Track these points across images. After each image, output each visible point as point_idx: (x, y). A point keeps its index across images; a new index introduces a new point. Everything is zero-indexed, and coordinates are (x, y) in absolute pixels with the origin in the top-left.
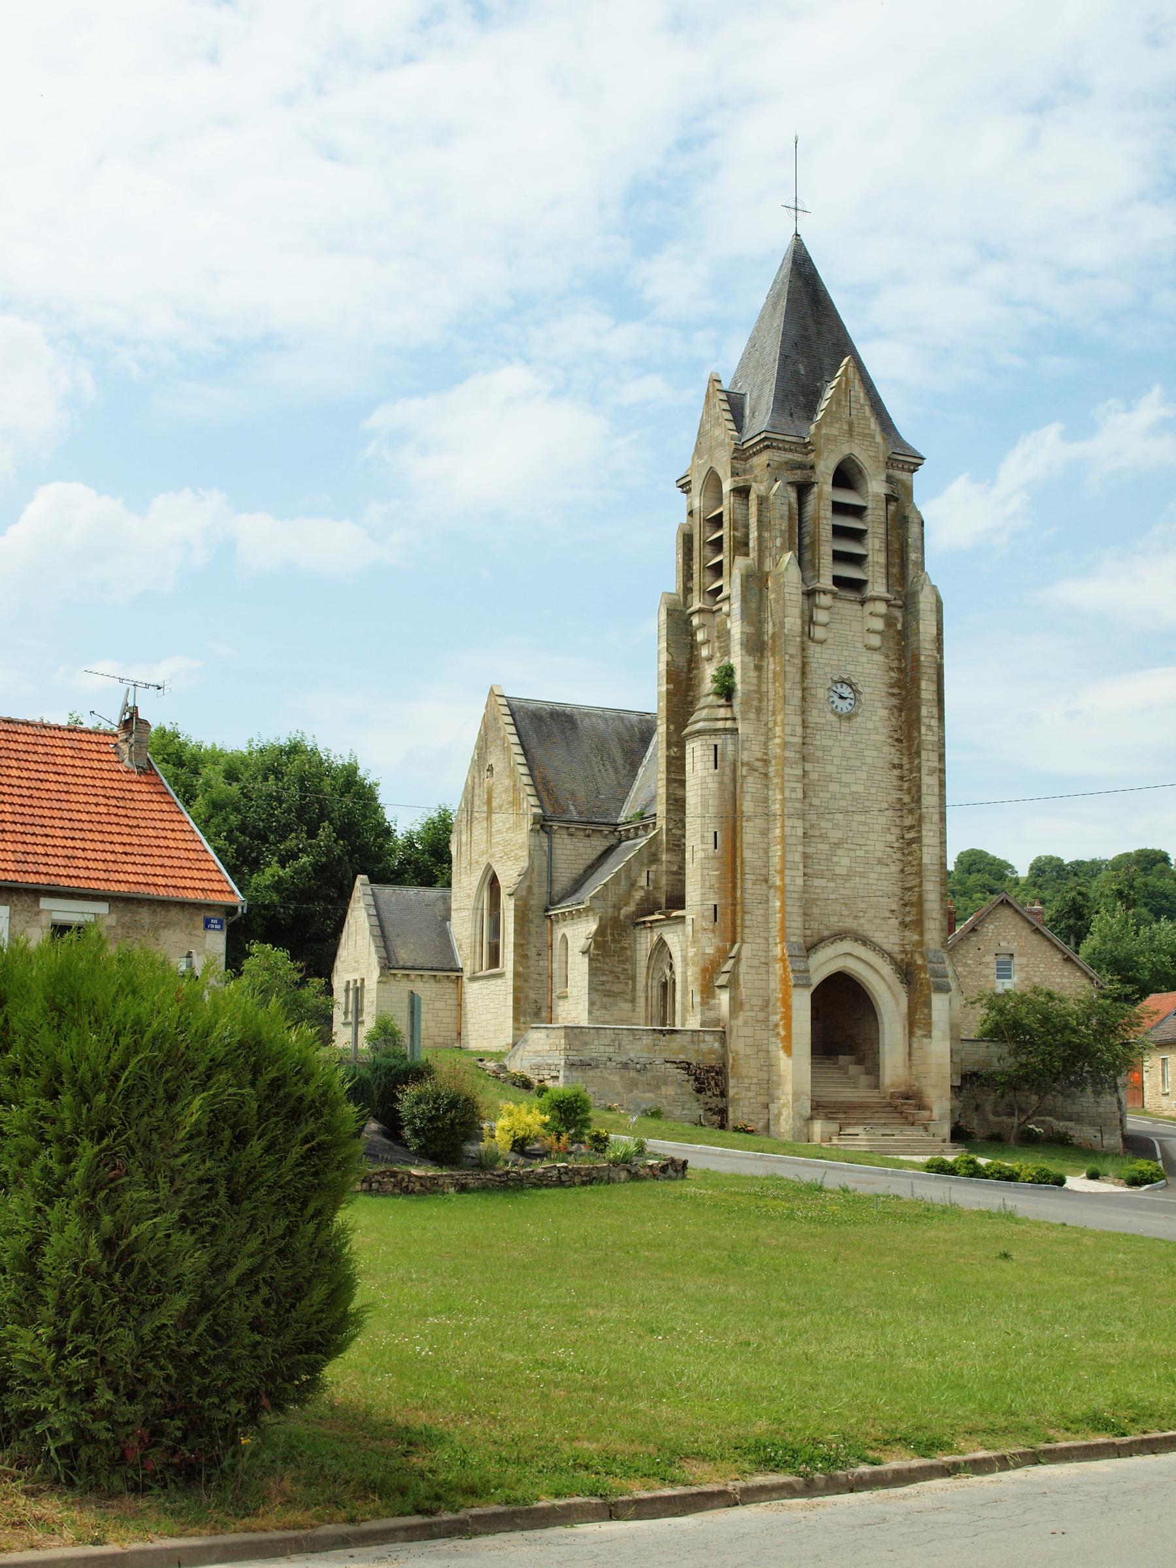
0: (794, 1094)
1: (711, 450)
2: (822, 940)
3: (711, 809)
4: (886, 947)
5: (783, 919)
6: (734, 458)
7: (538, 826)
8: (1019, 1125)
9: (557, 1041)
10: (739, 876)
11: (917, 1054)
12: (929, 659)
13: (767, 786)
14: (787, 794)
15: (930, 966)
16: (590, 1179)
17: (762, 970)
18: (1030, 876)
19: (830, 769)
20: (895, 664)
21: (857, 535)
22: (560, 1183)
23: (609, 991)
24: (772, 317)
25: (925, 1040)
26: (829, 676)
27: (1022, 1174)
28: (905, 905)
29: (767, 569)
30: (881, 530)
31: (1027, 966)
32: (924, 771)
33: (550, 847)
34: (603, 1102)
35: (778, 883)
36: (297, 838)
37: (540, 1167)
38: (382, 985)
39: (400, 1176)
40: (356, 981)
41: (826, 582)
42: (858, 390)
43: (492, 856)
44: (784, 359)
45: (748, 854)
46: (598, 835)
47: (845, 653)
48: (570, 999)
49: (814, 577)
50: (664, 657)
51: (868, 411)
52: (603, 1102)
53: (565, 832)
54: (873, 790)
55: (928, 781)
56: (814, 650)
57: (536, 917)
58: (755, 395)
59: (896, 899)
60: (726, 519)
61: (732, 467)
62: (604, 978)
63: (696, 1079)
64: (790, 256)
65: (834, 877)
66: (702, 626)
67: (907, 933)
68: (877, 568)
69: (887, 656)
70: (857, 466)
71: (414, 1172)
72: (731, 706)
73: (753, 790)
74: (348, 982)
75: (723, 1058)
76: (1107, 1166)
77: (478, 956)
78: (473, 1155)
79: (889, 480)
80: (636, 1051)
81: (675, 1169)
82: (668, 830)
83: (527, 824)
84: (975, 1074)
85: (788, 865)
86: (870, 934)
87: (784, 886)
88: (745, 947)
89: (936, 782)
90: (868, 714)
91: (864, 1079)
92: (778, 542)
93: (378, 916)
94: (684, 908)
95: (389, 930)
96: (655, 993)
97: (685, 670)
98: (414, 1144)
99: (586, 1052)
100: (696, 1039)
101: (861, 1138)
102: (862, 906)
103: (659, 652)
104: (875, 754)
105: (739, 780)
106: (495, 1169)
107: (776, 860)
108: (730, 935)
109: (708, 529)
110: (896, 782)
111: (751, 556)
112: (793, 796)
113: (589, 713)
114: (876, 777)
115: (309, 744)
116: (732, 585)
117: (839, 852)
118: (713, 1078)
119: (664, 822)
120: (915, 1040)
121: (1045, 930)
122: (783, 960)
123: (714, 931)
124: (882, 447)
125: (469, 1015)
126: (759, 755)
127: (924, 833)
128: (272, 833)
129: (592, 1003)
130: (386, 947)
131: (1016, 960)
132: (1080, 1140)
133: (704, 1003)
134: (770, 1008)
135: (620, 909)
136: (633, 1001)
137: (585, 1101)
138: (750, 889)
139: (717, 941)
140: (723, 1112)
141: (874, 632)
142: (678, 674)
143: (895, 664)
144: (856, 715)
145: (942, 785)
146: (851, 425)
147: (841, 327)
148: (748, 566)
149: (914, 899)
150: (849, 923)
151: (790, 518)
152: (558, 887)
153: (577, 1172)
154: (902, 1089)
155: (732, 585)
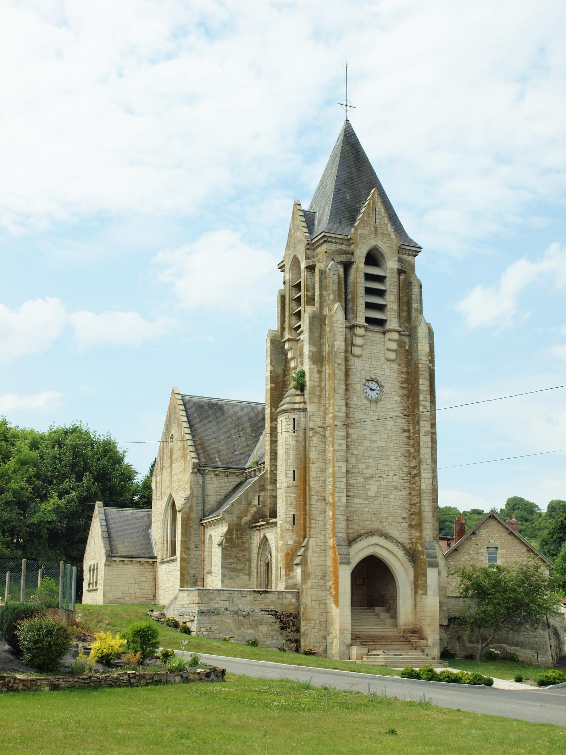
0: (340, 630)
1: (295, 244)
2: (360, 536)
3: (291, 457)
4: (400, 540)
5: (334, 523)
6: (307, 249)
7: (196, 470)
8: (482, 649)
9: (194, 598)
10: (307, 497)
11: (419, 605)
12: (425, 366)
13: (325, 443)
14: (336, 447)
15: (426, 551)
16: (156, 681)
17: (322, 554)
18: (548, 512)
19: (365, 432)
20: (405, 370)
21: (381, 293)
22: (130, 684)
23: (234, 568)
24: (332, 168)
25: (424, 597)
26: (364, 377)
27: (463, 678)
28: (412, 514)
29: (325, 313)
30: (395, 290)
31: (506, 554)
32: (422, 433)
33: (204, 483)
34: (221, 635)
35: (331, 501)
36: (70, 482)
37: (115, 673)
38: (107, 567)
39: (7, 680)
40: (94, 565)
41: (361, 321)
42: (380, 208)
43: (172, 489)
44: (337, 190)
45: (312, 483)
46: (233, 475)
47: (374, 363)
48: (213, 574)
49: (353, 318)
50: (269, 368)
51: (386, 220)
52: (221, 635)
53: (213, 473)
54: (391, 445)
55: (425, 440)
56: (354, 361)
57: (194, 524)
58: (321, 213)
59: (406, 511)
60: (302, 285)
61: (306, 254)
62: (231, 561)
63: (281, 621)
64: (343, 133)
65: (367, 498)
66: (291, 349)
67: (413, 531)
68: (392, 313)
69: (399, 365)
70: (380, 252)
71: (19, 676)
72: (304, 395)
73: (317, 445)
74: (91, 566)
75: (298, 608)
76: (530, 673)
77: (165, 549)
78: (67, 665)
79: (400, 260)
80: (243, 604)
81: (218, 675)
83: (190, 469)
84: (455, 618)
85: (337, 490)
86: (390, 532)
87: (334, 502)
88: (312, 540)
89: (430, 439)
90: (387, 399)
91: (389, 621)
92: (331, 297)
93: (107, 526)
94: (276, 517)
95: (113, 534)
96: (262, 570)
97: (282, 376)
98: (27, 657)
99: (211, 604)
100: (281, 596)
101: (380, 657)
102: (385, 515)
103: (266, 365)
104: (392, 423)
105: (308, 439)
106: (81, 675)
107: (330, 487)
108: (302, 533)
109: (294, 292)
110: (406, 440)
111: (316, 306)
112: (340, 448)
113: (232, 404)
114: (393, 437)
115: (84, 428)
116: (305, 324)
118: (291, 620)
119: (269, 466)
120: (418, 596)
121: (516, 533)
122: (334, 548)
123: (293, 531)
124: (395, 241)
125: (160, 585)
126: (320, 424)
127: (422, 470)
128: (55, 479)
129: (223, 576)
130: (110, 544)
131: (500, 551)
132: (524, 658)
133: (287, 574)
134: (327, 578)
135: (241, 519)
136: (249, 574)
137: (154, 631)
138: (315, 505)
139: (294, 537)
140: (297, 642)
141: (391, 350)
142: (277, 378)
143: (405, 370)
144: (380, 400)
145: (434, 441)
146: (376, 228)
147: (373, 173)
148: (313, 312)
149: (417, 510)
150: (376, 526)
151: (339, 283)
152: (208, 507)
153: (143, 677)
154: (411, 627)
155: (305, 324)
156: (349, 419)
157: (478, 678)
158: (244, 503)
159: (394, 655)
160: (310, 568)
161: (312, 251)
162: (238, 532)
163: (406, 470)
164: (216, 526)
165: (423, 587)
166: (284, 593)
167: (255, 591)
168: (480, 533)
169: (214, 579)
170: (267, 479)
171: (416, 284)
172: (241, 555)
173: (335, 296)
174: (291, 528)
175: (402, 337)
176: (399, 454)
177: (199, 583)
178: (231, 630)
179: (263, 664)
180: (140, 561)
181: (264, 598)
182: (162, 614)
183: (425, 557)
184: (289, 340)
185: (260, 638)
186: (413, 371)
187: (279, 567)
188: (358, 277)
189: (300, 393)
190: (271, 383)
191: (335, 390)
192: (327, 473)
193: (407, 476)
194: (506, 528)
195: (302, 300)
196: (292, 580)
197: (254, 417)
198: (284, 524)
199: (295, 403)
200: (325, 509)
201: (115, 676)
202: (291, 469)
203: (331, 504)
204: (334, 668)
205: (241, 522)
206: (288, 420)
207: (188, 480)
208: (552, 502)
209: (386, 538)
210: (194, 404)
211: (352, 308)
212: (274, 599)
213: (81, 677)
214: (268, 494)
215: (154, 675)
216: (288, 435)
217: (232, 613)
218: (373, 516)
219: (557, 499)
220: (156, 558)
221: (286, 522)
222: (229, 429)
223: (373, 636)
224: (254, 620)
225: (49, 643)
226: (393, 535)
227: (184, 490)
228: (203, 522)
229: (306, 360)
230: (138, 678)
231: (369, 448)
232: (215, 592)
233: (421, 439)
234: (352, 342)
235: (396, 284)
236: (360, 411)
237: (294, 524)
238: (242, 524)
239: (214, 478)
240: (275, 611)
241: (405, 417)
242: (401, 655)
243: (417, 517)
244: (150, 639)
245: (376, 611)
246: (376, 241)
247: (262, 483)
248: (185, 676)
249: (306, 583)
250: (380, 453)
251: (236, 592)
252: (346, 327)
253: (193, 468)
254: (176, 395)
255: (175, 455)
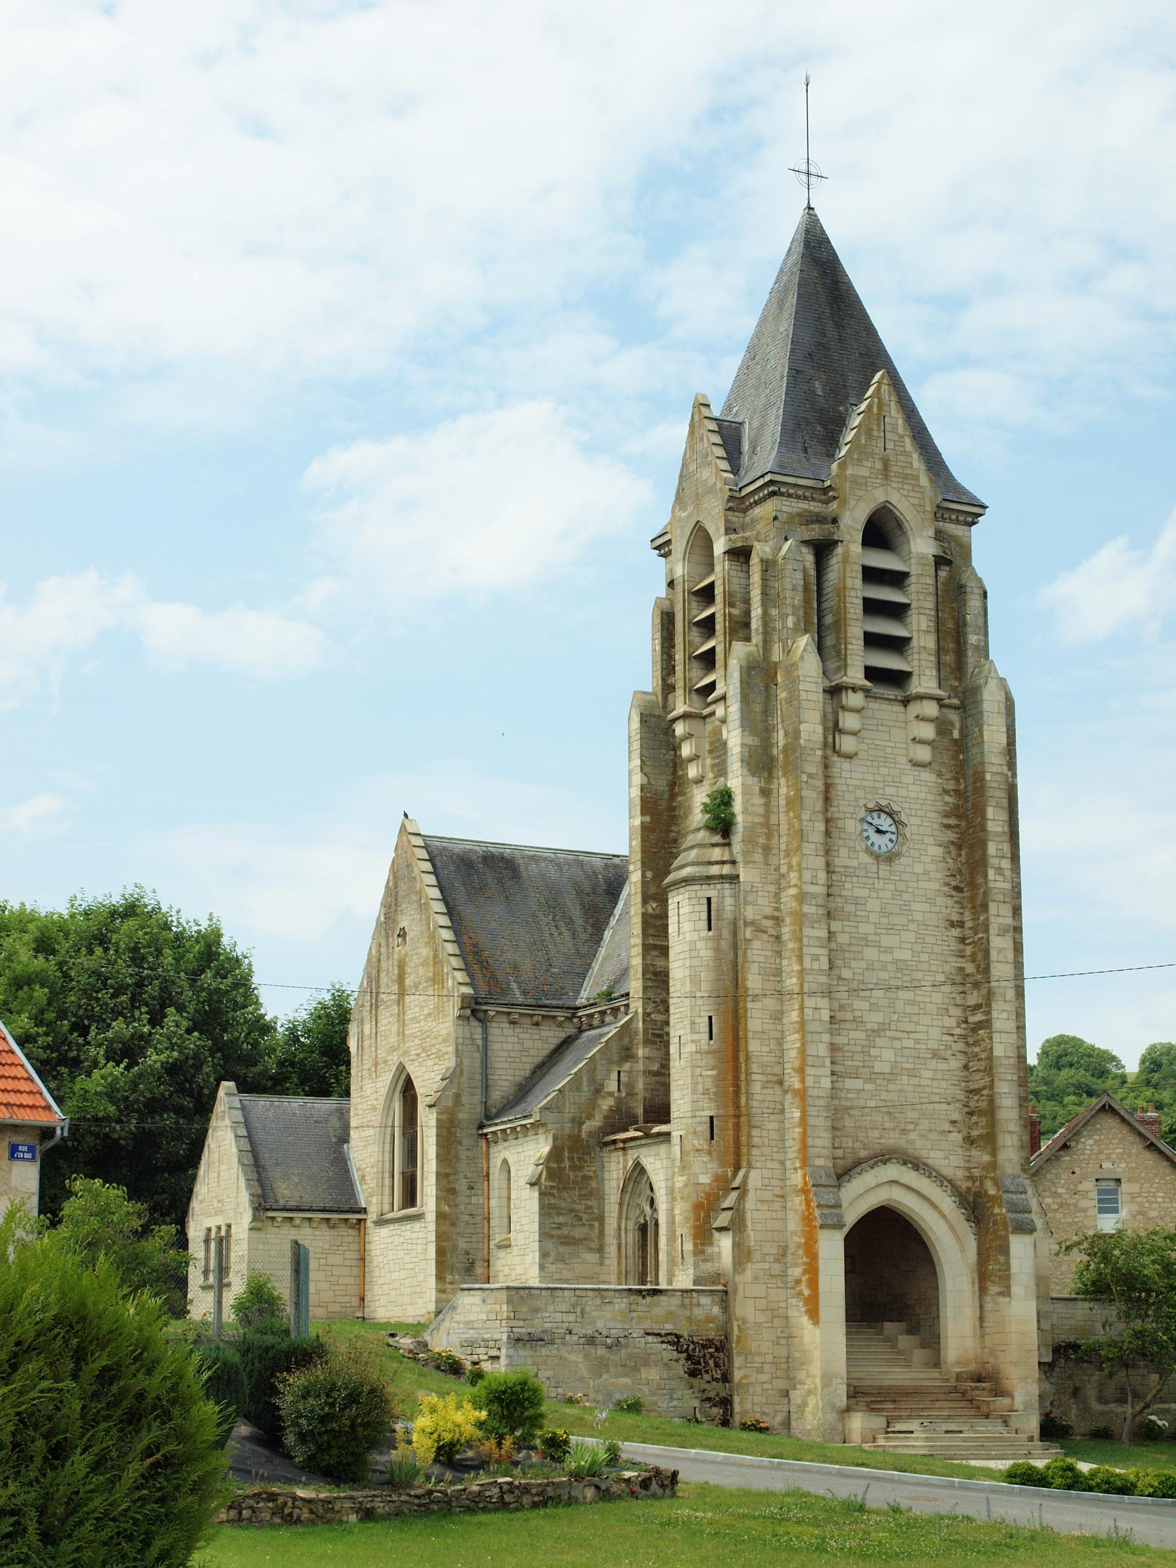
1: (698, 497)
2: (858, 1163)
3: (704, 986)
4: (946, 1171)
5: (804, 1134)
6: (730, 509)
7: (468, 1012)
9: (497, 1307)
10: (743, 1077)
12: (998, 778)
15: (1006, 1196)
16: (545, 1499)
18: (1141, 1072)
19: (865, 929)
20: (951, 785)
21: (897, 611)
25: (1001, 1299)
26: (862, 802)
27: (1139, 1484)
28: (971, 1114)
30: (929, 604)
32: (993, 930)
33: (485, 1040)
34: (560, 1390)
35: (797, 1086)
38: (255, 1234)
40: (219, 1228)
41: (855, 675)
44: (795, 374)
45: (754, 1046)
46: (550, 1022)
47: (883, 771)
48: (515, 1250)
49: (839, 669)
50: (638, 779)
51: (908, 444)
52: (560, 1390)
53: (504, 1018)
54: (924, 957)
55: (999, 944)
56: (840, 767)
57: (465, 1135)
58: (756, 424)
59: (959, 1105)
60: (718, 591)
61: (727, 521)
62: (561, 1219)
63: (689, 1358)
64: (801, 237)
65: (872, 1077)
66: (688, 736)
67: (974, 1152)
68: (924, 656)
71: (301, 1493)
72: (729, 845)
73: (761, 959)
74: (209, 1230)
77: (387, 1190)
79: (939, 536)
81: (661, 1483)
82: (646, 1015)
83: (453, 1009)
85: (810, 1061)
86: (924, 1154)
88: (753, 1174)
91: (919, 1355)
92: (790, 622)
94: (668, 1121)
95: (265, 1156)
97: (666, 796)
98: (300, 1454)
100: (687, 1301)
102: (912, 1115)
103: (630, 772)
104: (926, 907)
105: (742, 945)
106: (411, 1487)
107: (792, 1055)
108: (731, 1158)
109: (694, 605)
110: (955, 946)
111: (754, 640)
112: (816, 966)
113: (536, 857)
115: (149, 901)
117: (879, 1042)
118: (712, 1356)
119: (640, 1004)
120: (988, 1299)
122: (805, 1191)
123: (710, 1153)
126: (768, 911)
127: (995, 1014)
129: (544, 1255)
131: (1125, 1187)
133: (698, 1252)
134: (789, 1259)
135: (581, 1124)
136: (601, 1250)
138: (759, 1094)
139: (714, 1167)
143: (951, 785)
144: (899, 855)
145: (1018, 948)
146: (886, 463)
148: (749, 655)
149: (983, 1105)
150: (893, 1140)
151: (806, 588)
152: (496, 1095)
153: (526, 1489)
154: (972, 1367)
155: (729, 680)
156: (831, 899)
157: (1169, 1483)
158: (585, 1089)
159: (946, 1432)
160: (752, 1236)
161: (742, 515)
162: (575, 1156)
163: (957, 1012)
164: (520, 1141)
165: (1000, 1278)
166: (695, 1294)
167: (630, 1290)
168: (1080, 1146)
169: (517, 1260)
170: (636, 1033)
171: (976, 591)
172: (582, 1207)
173: (798, 621)
174: (706, 1147)
175: (944, 710)
176: (941, 978)
177: (479, 1270)
178: (581, 1379)
179: (698, 1457)
180: (328, 1220)
181: (650, 1306)
182: (419, 1343)
183: (1004, 1211)
184: (685, 716)
185: (645, 1394)
186: (970, 789)
187: (678, 1234)
188: (848, 575)
189: (722, 841)
190: (642, 814)
191: (801, 835)
192: (785, 1021)
193: (958, 1026)
194: (1140, 1134)
195: (719, 626)
196: (709, 1264)
197: (587, 887)
198: (690, 1137)
199: (710, 863)
200: (782, 1104)
201: (475, 1488)
202: (703, 1013)
203: (797, 1093)
204: (857, 1465)
205: (580, 1131)
206: (694, 902)
207: (448, 1035)
208: (1152, 1049)
209: (916, 1167)
210: (451, 857)
211: (834, 646)
212: (674, 1308)
213: (412, 1493)
214: (640, 1066)
215: (547, 1485)
216: (695, 936)
217: (582, 1341)
218: (886, 1118)
219: (1165, 1040)
220: (365, 1210)
221: (695, 1132)
222: (534, 916)
223: (890, 1387)
224: (630, 1356)
225: (353, 1421)
226: (930, 1162)
227: (440, 1056)
228: (485, 1131)
229: (735, 767)
230: (517, 1491)
231: (877, 965)
232: (544, 1293)
233: (992, 945)
234: (836, 723)
235: (932, 589)
236: (855, 879)
237: (712, 1138)
238: (584, 1135)
239: (508, 1030)
240: (677, 1336)
241: (954, 893)
242: (961, 1432)
243: (983, 1121)
244: (526, 1409)
245: (886, 1332)
246: (886, 492)
247: (626, 1041)
248: (603, 1488)
249: (744, 1270)
250: (900, 975)
251: (590, 1293)
252: (824, 691)
253: (462, 1008)
254: (411, 837)
255: (412, 977)
